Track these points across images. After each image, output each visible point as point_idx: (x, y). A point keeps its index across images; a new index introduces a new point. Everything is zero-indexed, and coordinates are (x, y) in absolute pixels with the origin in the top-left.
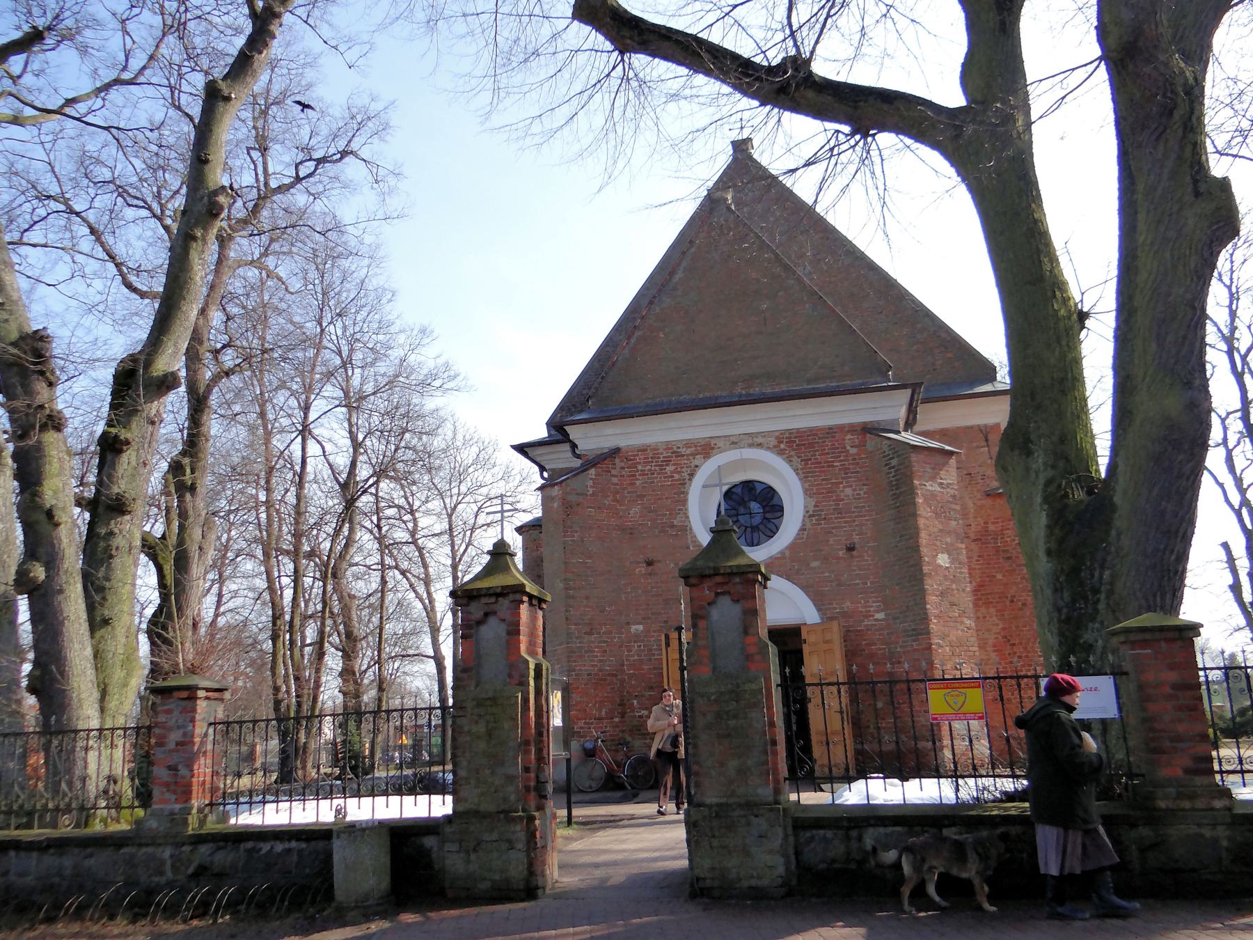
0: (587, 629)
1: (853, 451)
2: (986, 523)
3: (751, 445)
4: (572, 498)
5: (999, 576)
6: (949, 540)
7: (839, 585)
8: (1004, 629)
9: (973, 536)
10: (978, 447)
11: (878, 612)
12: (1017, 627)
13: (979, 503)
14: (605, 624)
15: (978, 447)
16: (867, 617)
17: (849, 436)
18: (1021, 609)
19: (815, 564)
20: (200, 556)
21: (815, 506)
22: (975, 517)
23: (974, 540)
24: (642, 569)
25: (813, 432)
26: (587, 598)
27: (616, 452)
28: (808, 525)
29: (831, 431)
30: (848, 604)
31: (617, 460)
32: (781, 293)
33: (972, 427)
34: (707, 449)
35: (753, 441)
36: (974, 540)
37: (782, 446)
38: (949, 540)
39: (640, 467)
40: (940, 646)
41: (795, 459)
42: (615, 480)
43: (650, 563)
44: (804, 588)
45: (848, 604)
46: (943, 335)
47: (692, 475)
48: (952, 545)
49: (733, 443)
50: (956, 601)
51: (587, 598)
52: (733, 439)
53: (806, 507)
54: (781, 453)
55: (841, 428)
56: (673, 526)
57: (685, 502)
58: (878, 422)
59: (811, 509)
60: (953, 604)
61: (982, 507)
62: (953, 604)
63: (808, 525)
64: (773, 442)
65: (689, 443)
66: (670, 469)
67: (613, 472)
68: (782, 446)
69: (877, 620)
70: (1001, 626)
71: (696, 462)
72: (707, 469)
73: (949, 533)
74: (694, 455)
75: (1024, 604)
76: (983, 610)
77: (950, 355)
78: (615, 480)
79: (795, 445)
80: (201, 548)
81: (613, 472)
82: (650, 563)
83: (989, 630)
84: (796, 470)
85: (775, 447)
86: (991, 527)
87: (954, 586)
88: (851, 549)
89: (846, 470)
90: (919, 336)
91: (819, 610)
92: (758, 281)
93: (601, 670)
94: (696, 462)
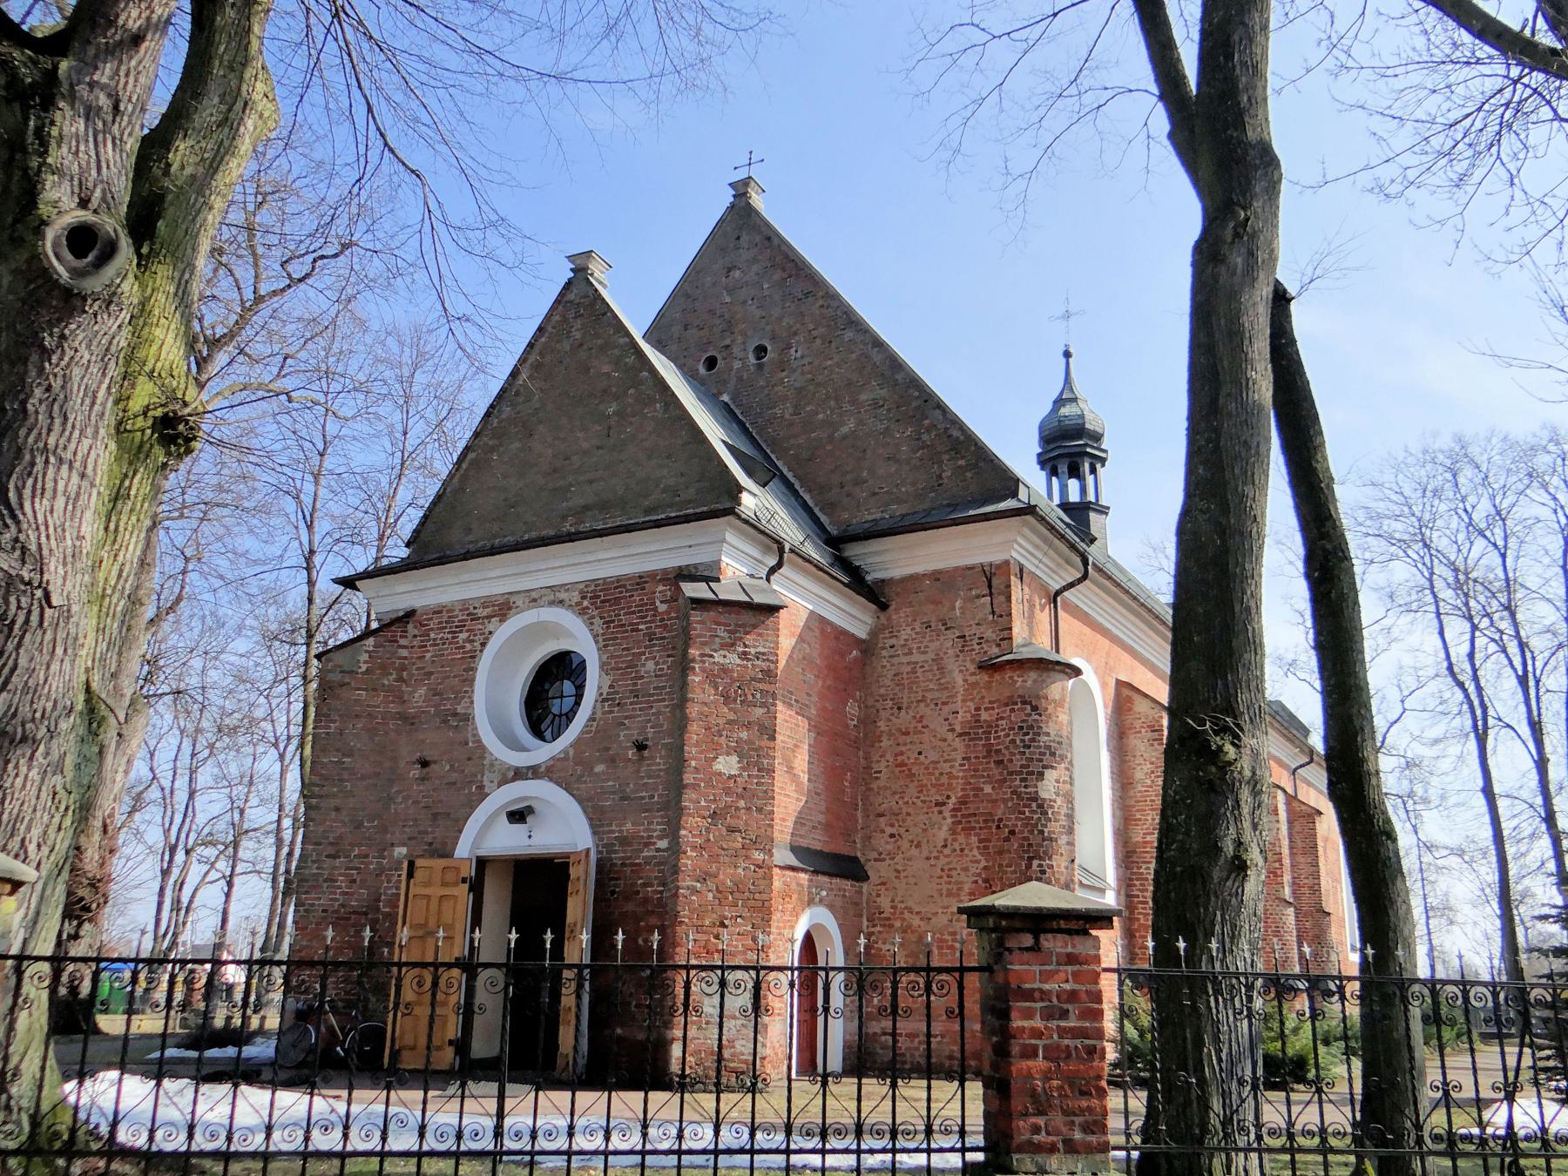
0: (330, 850)
1: (662, 608)
2: (977, 709)
3: (552, 603)
4: (335, 677)
5: (988, 789)
6: (744, 735)
7: (623, 799)
8: (985, 868)
9: (958, 729)
10: (978, 597)
11: (661, 838)
12: (1000, 866)
13: (972, 679)
14: (360, 845)
15: (978, 597)
16: (647, 845)
17: (661, 588)
18: (1007, 839)
19: (599, 768)
20: (118, 744)
21: (611, 686)
22: (964, 701)
23: (960, 735)
24: (416, 772)
25: (619, 583)
26: (337, 809)
27: (410, 614)
28: (599, 715)
29: (641, 580)
30: (629, 826)
31: (410, 626)
32: (631, 391)
33: (971, 568)
34: (503, 608)
35: (553, 596)
36: (960, 735)
37: (586, 603)
38: (744, 735)
39: (432, 635)
40: (695, 891)
41: (597, 621)
42: (404, 653)
43: (424, 764)
44: (580, 801)
45: (629, 826)
46: (956, 433)
47: (483, 645)
48: (749, 742)
49: (535, 600)
50: (741, 825)
51: (337, 809)
52: (534, 595)
53: (600, 688)
54: (582, 612)
55: (652, 575)
56: (455, 714)
57: (471, 681)
58: (695, 566)
59: (605, 690)
60: (732, 830)
61: (974, 685)
62: (732, 830)
63: (599, 715)
64: (576, 596)
65: (486, 602)
66: (463, 636)
67: (403, 642)
68: (586, 603)
69: (658, 850)
70: (984, 863)
71: (491, 627)
72: (503, 632)
73: (748, 726)
74: (489, 617)
75: (1012, 832)
76: (961, 839)
77: (962, 462)
78: (404, 653)
79: (602, 600)
80: (120, 735)
81: (403, 642)
82: (424, 764)
83: (966, 869)
84: (595, 637)
85: (577, 604)
86: (984, 716)
87: (742, 804)
88: (641, 747)
89: (651, 636)
90: (925, 437)
91: (594, 833)
92: (608, 375)
93: (343, 906)
94: (491, 627)
